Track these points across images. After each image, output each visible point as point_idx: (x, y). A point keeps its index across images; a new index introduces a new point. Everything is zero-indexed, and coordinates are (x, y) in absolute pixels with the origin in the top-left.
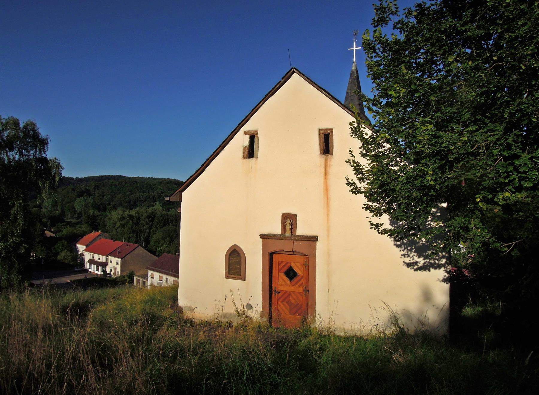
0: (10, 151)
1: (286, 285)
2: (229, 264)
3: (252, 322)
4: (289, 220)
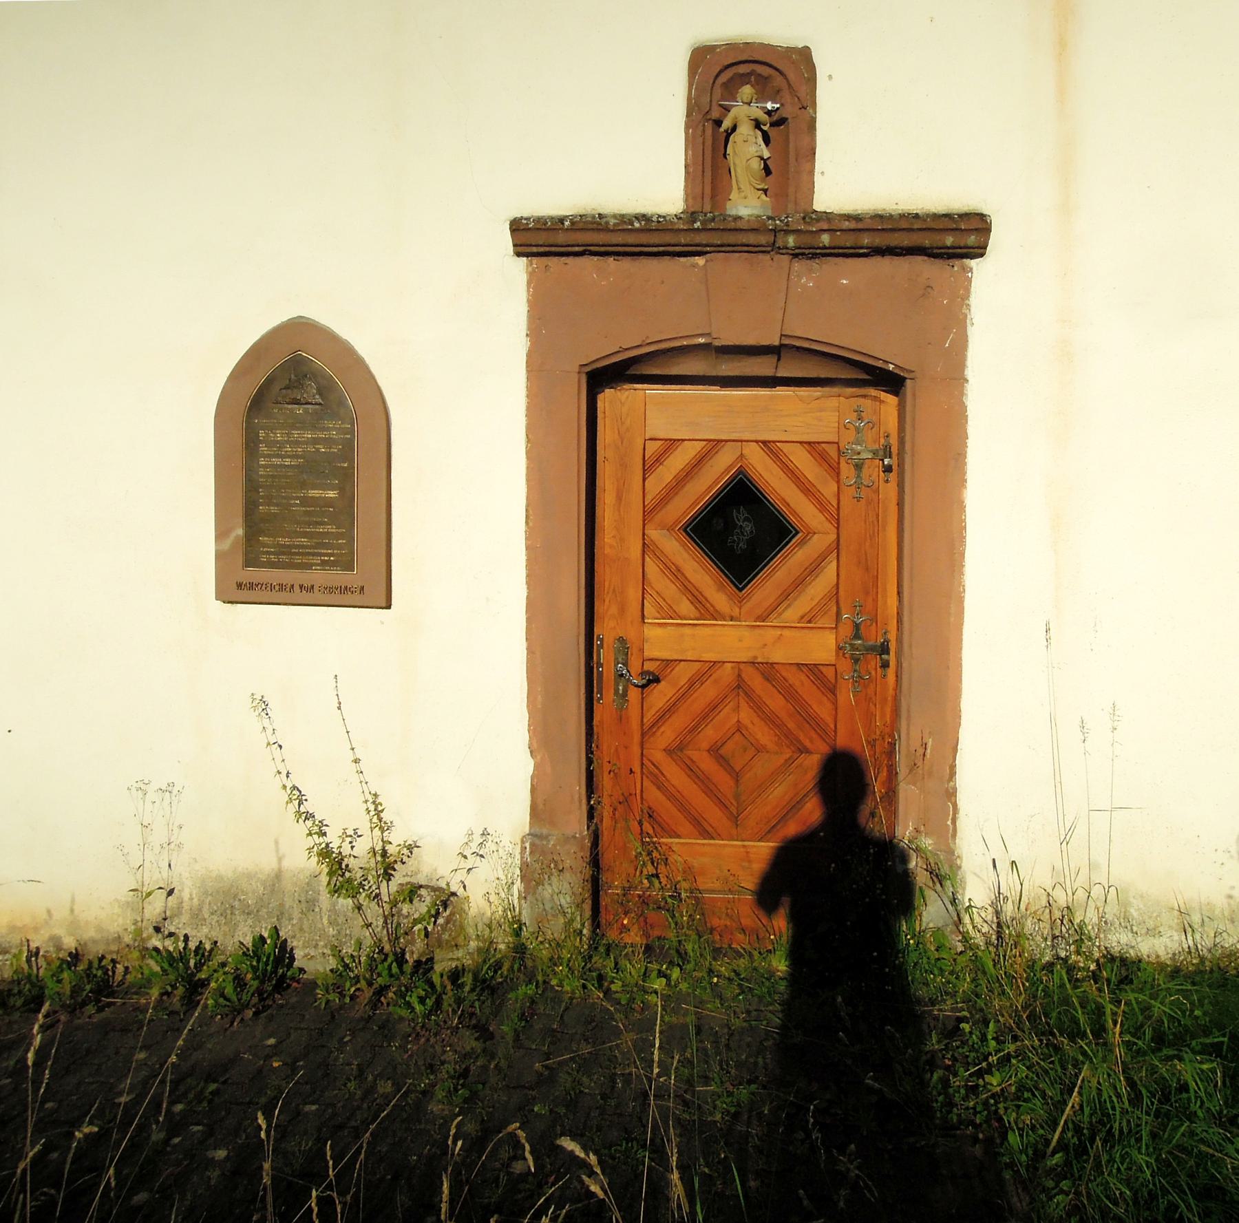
0: (685, 1026)
1: (706, 611)
2: (251, 486)
3: (457, 925)
4: (752, 95)
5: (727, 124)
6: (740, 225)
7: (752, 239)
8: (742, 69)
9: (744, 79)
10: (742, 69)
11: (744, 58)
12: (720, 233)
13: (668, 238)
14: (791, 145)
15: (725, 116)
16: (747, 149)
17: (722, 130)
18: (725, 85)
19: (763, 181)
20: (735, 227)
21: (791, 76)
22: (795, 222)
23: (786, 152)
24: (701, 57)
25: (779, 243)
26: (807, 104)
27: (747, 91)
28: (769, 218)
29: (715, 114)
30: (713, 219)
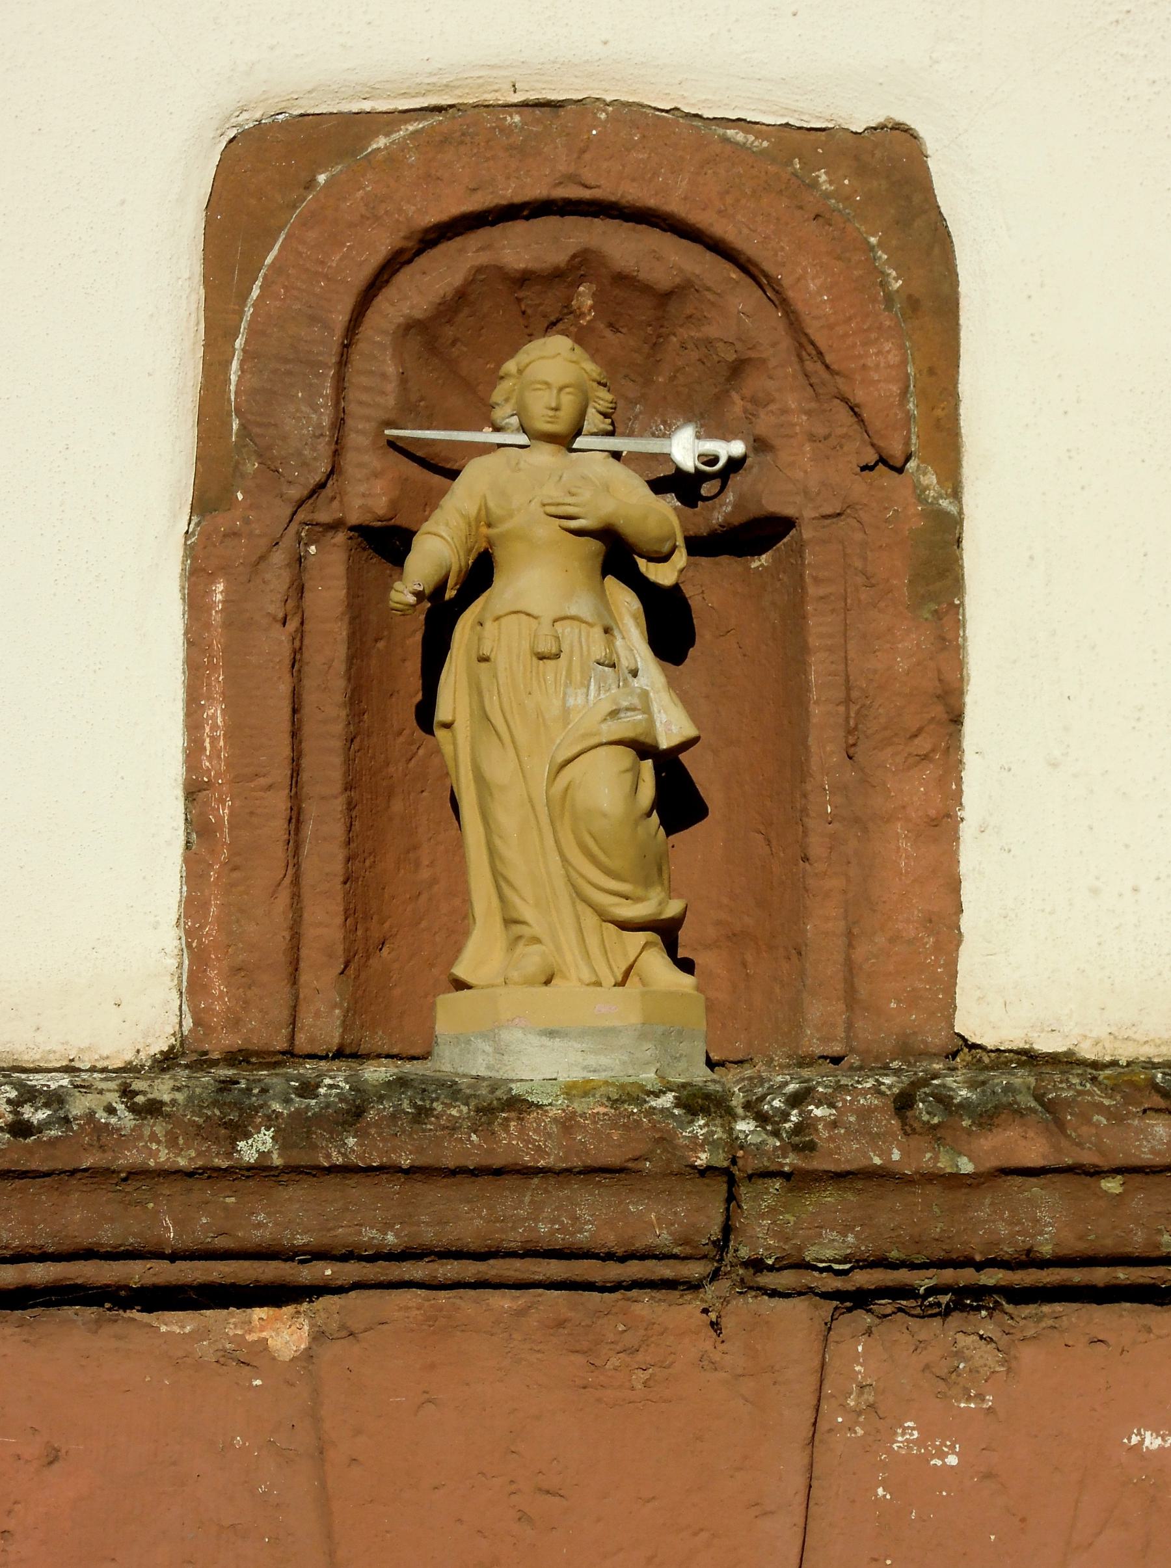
5: (434, 553)
6: (512, 1142)
7: (589, 1217)
8: (520, 248)
9: (536, 301)
10: (520, 248)
11: (536, 190)
12: (394, 1187)
13: (78, 1217)
14: (818, 669)
15: (429, 503)
16: (557, 699)
17: (403, 593)
18: (426, 334)
19: (654, 870)
20: (483, 1148)
21: (812, 287)
22: (851, 1123)
23: (792, 696)
24: (273, 175)
25: (760, 1235)
26: (910, 438)
27: (550, 367)
28: (696, 1102)
29: (368, 494)
30: (353, 1112)
